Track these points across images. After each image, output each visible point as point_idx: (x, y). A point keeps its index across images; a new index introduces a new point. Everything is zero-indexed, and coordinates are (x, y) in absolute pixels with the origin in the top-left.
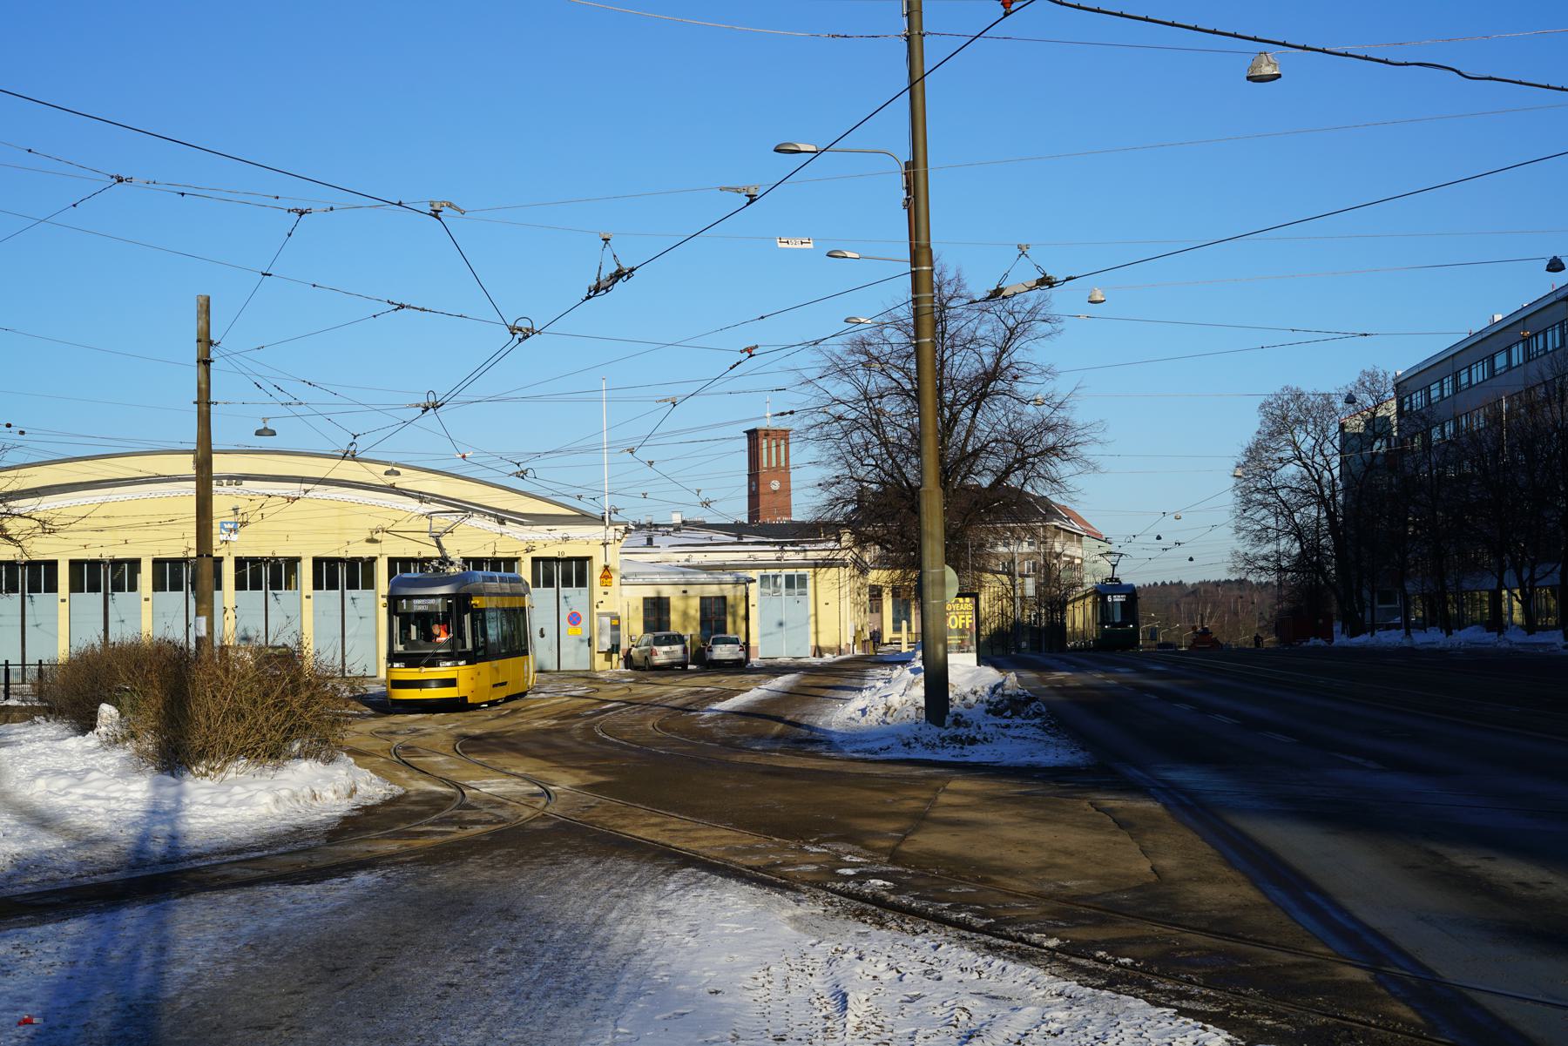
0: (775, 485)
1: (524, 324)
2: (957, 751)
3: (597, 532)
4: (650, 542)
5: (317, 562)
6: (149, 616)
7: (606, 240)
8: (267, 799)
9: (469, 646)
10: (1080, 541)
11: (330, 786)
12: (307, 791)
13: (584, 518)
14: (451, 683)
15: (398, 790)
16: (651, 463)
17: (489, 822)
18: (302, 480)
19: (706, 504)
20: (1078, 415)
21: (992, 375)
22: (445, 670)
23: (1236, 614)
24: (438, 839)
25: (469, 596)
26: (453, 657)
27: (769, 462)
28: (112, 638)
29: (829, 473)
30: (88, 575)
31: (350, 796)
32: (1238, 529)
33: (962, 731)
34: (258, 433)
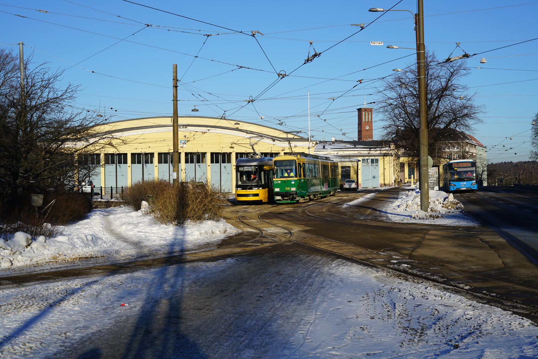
0: (367, 128)
1: (283, 73)
2: (432, 220)
3: (306, 144)
4: (324, 147)
5: (212, 154)
6: (157, 172)
7: (311, 43)
8: (197, 233)
9: (263, 182)
10: (475, 147)
11: (218, 229)
12: (210, 231)
13: (302, 139)
14: (257, 195)
15: (240, 231)
16: (325, 120)
17: (271, 242)
18: (207, 126)
19: (344, 134)
20: (476, 103)
21: (445, 88)
22: (255, 191)
23: (531, 173)
24: (254, 248)
25: (263, 166)
26: (258, 186)
27: (365, 120)
28: (145, 179)
29: (387, 123)
30: (137, 158)
31: (224, 233)
32: (533, 143)
33: (434, 214)
34: (193, 110)
